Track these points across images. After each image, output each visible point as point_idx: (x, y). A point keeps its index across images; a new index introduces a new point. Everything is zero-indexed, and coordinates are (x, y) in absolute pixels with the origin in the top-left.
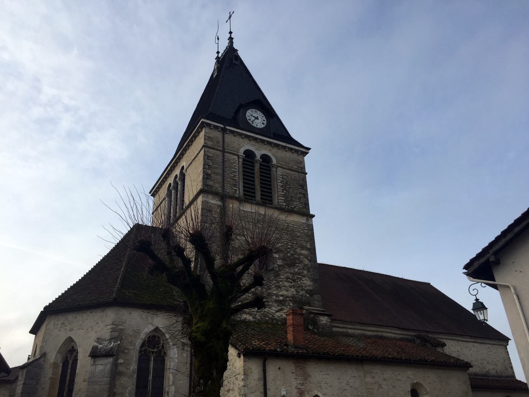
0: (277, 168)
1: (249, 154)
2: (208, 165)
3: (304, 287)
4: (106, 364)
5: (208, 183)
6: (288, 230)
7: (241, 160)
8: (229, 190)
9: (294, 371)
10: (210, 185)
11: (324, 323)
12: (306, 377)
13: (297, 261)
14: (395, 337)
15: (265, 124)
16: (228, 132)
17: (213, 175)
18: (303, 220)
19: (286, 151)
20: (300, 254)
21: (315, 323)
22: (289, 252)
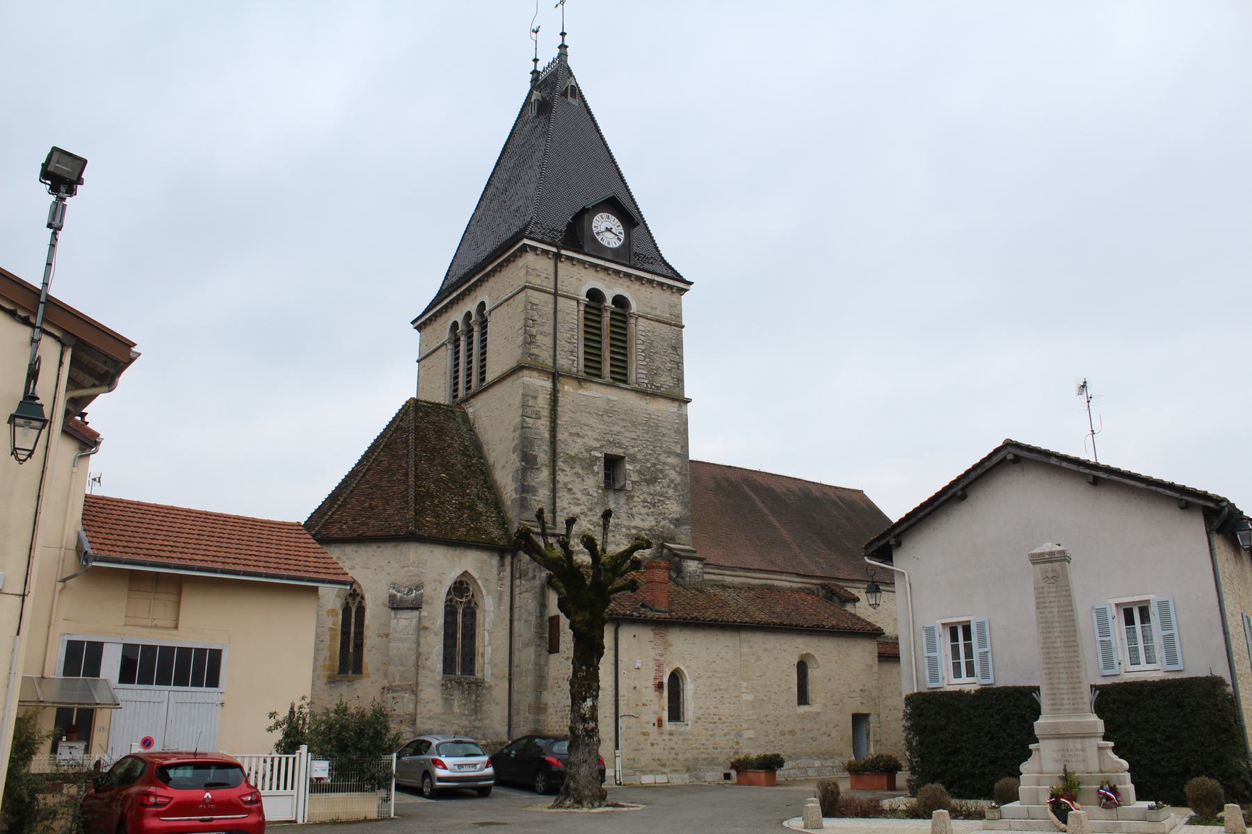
0: (637, 318)
1: (595, 295)
2: (533, 318)
3: (667, 515)
4: (411, 619)
5: (531, 351)
6: (651, 426)
7: (582, 308)
8: (564, 362)
9: (652, 639)
10: (534, 355)
11: (693, 570)
12: (667, 646)
13: (660, 476)
14: (791, 587)
15: (623, 239)
16: (563, 260)
17: (539, 337)
18: (672, 407)
19: (654, 287)
20: (664, 463)
21: (679, 570)
22: (647, 460)
